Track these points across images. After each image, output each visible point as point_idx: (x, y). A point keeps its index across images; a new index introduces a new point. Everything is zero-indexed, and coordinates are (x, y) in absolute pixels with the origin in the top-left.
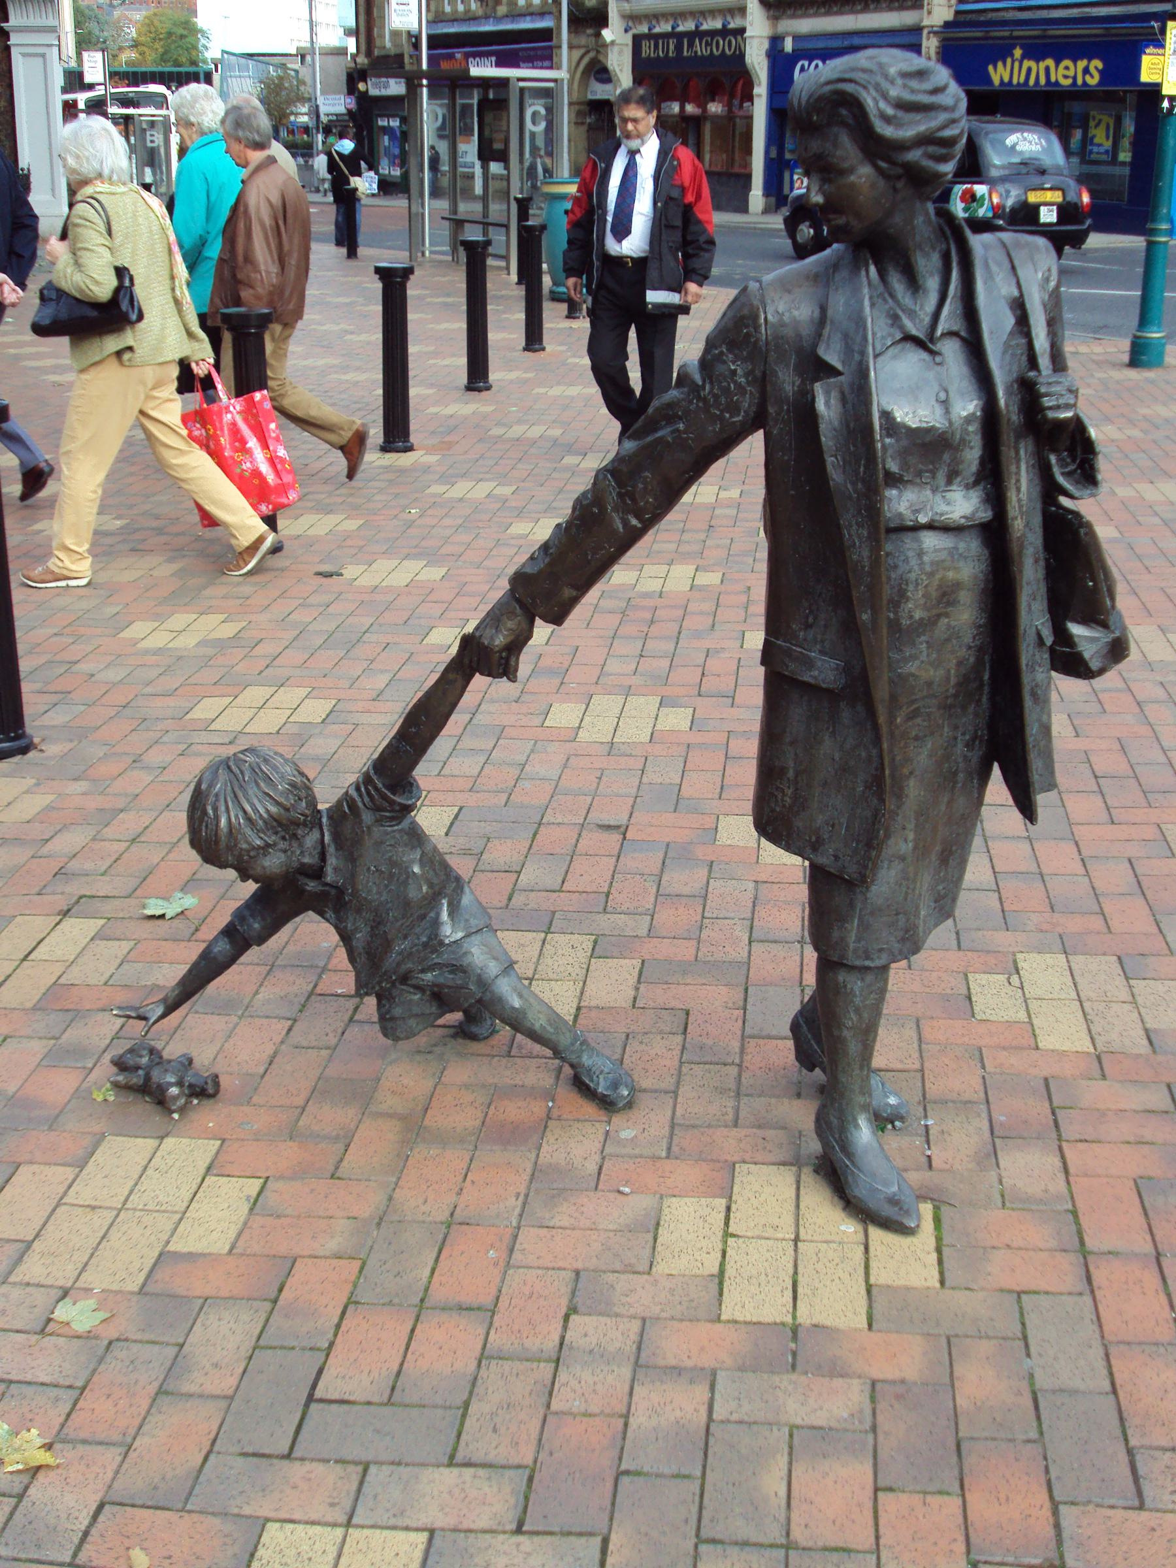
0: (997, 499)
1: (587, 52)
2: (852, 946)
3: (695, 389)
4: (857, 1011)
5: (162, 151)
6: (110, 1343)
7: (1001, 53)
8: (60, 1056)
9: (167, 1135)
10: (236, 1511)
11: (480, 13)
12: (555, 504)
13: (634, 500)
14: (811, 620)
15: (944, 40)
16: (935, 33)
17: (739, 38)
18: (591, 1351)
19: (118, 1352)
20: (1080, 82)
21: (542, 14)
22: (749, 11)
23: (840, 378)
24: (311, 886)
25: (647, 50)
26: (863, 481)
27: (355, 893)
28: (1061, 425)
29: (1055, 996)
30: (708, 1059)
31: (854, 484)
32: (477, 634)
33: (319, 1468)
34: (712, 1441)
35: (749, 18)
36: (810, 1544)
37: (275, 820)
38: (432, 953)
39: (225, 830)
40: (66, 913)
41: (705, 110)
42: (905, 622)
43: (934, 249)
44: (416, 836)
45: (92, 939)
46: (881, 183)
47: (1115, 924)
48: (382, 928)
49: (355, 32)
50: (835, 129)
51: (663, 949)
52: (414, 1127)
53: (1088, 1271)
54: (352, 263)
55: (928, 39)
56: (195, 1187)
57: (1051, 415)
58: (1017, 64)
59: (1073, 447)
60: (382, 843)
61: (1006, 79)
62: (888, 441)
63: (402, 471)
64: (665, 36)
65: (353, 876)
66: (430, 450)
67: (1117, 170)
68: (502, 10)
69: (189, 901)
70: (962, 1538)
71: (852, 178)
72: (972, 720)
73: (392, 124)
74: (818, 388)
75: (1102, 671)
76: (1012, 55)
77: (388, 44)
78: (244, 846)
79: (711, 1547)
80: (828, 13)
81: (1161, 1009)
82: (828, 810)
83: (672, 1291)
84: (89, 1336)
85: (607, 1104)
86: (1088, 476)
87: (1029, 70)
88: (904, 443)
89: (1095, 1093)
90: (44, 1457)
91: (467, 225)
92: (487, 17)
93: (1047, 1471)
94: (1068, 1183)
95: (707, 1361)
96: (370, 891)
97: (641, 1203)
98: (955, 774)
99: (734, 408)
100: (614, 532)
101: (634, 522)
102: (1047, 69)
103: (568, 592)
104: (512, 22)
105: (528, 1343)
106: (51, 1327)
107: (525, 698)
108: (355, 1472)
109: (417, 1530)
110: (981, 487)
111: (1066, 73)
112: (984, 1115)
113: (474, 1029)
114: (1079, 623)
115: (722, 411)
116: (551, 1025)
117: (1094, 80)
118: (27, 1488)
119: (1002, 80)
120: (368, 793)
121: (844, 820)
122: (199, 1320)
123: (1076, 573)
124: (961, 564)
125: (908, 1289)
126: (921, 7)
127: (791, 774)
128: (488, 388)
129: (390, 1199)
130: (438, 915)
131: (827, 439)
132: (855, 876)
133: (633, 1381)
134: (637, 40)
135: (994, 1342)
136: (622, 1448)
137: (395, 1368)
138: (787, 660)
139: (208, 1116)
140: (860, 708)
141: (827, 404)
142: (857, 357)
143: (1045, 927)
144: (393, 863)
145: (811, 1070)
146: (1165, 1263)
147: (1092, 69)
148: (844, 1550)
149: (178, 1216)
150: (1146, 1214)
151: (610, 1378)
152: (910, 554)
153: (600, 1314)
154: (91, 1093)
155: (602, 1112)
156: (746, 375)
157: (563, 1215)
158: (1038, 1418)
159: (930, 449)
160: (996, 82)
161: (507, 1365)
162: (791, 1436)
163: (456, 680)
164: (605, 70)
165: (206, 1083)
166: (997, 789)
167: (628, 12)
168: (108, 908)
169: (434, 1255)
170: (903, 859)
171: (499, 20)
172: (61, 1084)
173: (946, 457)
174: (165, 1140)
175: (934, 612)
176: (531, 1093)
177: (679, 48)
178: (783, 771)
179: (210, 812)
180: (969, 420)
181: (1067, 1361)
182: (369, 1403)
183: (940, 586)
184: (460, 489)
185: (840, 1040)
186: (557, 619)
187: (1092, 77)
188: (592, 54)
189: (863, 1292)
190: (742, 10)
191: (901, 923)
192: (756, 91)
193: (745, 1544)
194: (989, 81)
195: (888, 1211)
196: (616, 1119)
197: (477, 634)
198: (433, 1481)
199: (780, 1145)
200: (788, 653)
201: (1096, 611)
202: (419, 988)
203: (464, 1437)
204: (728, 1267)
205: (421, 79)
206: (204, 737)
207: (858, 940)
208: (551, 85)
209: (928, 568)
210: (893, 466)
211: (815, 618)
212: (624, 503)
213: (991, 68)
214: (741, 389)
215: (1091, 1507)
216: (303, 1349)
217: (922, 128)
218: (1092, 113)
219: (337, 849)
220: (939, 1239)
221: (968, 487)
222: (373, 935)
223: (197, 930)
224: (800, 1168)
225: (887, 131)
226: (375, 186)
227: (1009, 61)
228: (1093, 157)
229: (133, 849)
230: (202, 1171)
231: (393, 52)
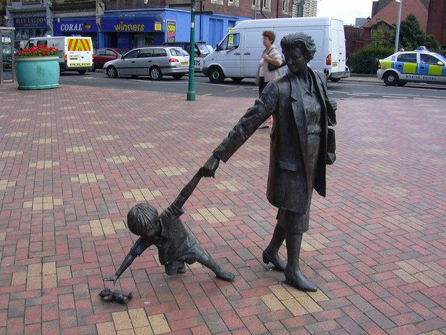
24: (157, 238)
85: (229, 280)
107: (14, 201)
117: (142, 30)
134: (15, 19)
159: (313, 115)
186: (225, 161)
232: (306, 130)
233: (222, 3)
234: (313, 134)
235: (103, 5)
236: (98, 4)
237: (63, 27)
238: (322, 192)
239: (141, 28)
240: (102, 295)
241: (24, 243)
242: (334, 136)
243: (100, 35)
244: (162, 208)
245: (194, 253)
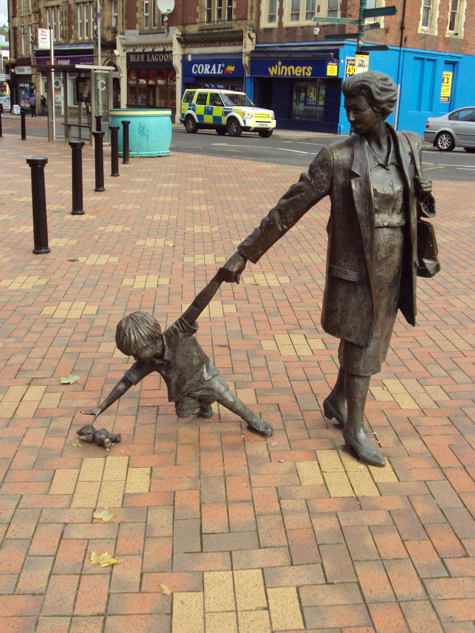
0: (407, 217)
1: (108, 59)
2: (361, 369)
3: (309, 182)
4: (361, 392)
6: (119, 524)
7: (273, 63)
8: (50, 432)
9: (107, 456)
10: (191, 570)
11: (63, 42)
12: (150, 233)
13: (286, 219)
14: (347, 258)
15: (251, 57)
16: (247, 55)
17: (170, 55)
18: (292, 510)
19: (122, 526)
20: (304, 75)
21: (89, 43)
22: (174, 44)
23: (360, 178)
24: (158, 361)
25: (132, 58)
26: (368, 211)
27: (175, 364)
29: (400, 392)
30: (291, 418)
31: (365, 213)
32: (226, 267)
33: (214, 555)
34: (344, 532)
35: (174, 47)
36: (389, 558)
37: (151, 336)
38: (201, 384)
39: (134, 341)
40: (29, 384)
41: (156, 83)
42: (379, 258)
43: (385, 136)
44: (195, 342)
45: (44, 393)
46: (374, 114)
47: (411, 369)
48: (183, 376)
50: (361, 97)
51: (260, 385)
52: (198, 447)
53: (444, 473)
54: (22, 142)
55: (245, 57)
56: (126, 472)
57: (425, 190)
58: (279, 68)
59: (428, 201)
60: (185, 344)
61: (276, 73)
62: (375, 198)
63: (84, 222)
64: (140, 53)
65: (174, 356)
66: (91, 214)
67: (318, 108)
68: (72, 41)
69: (76, 378)
70: (435, 552)
71: (365, 113)
72: (395, 291)
73: (26, 86)
74: (353, 182)
75: (434, 275)
76: (278, 64)
77: (24, 54)
78: (140, 346)
79: (357, 562)
81: (436, 394)
82: (353, 323)
83: (311, 490)
84: (110, 522)
85: (263, 434)
86: (432, 210)
87: (284, 70)
88: (380, 199)
89: (424, 421)
90: (114, 561)
91: (72, 127)
92: (66, 44)
93: (453, 530)
94: (427, 448)
95: (332, 509)
96: (179, 362)
97: (287, 465)
98: (391, 310)
99: (322, 188)
100: (279, 230)
101: (285, 227)
102: (291, 70)
103: (260, 252)
104: (76, 46)
105: (269, 510)
106: (94, 521)
108: (228, 555)
109: (257, 569)
110: (401, 214)
111: (299, 71)
112: (392, 430)
113: (206, 414)
114: (426, 259)
115: (318, 189)
116: (243, 408)
117: (309, 74)
118: (112, 571)
119: (274, 73)
120: (182, 326)
121: (359, 326)
122: (148, 514)
124: (396, 239)
125: (389, 483)
126: (242, 45)
127: (339, 311)
128: (104, 190)
129: (200, 470)
130: (203, 370)
131: (356, 198)
132: (364, 344)
133: (310, 518)
134: (128, 55)
135: (422, 496)
136: (316, 538)
137: (227, 522)
138: (338, 273)
139: (118, 448)
140: (365, 288)
141: (355, 186)
142: (365, 171)
143: (388, 371)
144: (188, 352)
145: (330, 418)
146: (467, 469)
147: (308, 70)
148: (400, 559)
149: (124, 482)
150: (456, 456)
151: (302, 517)
152: (381, 236)
153: (290, 499)
154: (72, 444)
155: (262, 438)
156: (326, 177)
157: (263, 470)
158: (445, 516)
159: (387, 200)
160: (272, 74)
161: (266, 517)
162: (369, 528)
163: (216, 284)
165: (117, 437)
167: (125, 44)
168: (46, 381)
169: (224, 486)
170: (377, 338)
171: (71, 45)
172: (57, 443)
173: (392, 204)
174: (107, 458)
175: (388, 255)
176: (235, 433)
177: (145, 58)
178: (336, 311)
179: (128, 335)
180: (399, 191)
181: (448, 499)
182: (223, 533)
183: (390, 247)
184: (110, 229)
185: (355, 403)
187: (308, 73)
188: (110, 60)
189: (374, 485)
190: (171, 44)
191: (376, 361)
192: (177, 75)
193: (368, 560)
194: (270, 74)
195: (374, 460)
196: (268, 439)
197: (226, 267)
198: (256, 553)
199: (328, 444)
200: (339, 270)
201: (432, 256)
202: (194, 398)
203: (260, 540)
204: (327, 481)
205: (51, 68)
206: (52, 321)
207: (363, 367)
208: (108, 72)
209: (386, 240)
210: (376, 207)
211: (349, 258)
212: (282, 220)
213: (269, 69)
214: (325, 182)
215: (471, 539)
216: (192, 519)
217: (388, 96)
218: (308, 87)
219: (168, 347)
220: (392, 467)
221: (398, 214)
222: (179, 378)
223: (84, 387)
224: (337, 450)
226: (19, 111)
227: (276, 66)
228: (309, 103)
229: (45, 360)
230: (126, 467)
231: (26, 57)
232: (371, 221)
233: (436, 33)
234: (387, 227)
235: (253, 35)
236: (246, 35)
237: (196, 69)
238: (411, 318)
239: (305, 71)
240: (80, 433)
241: (18, 359)
242: (44, 179)
243: (248, 81)
244: (167, 320)
245: (212, 389)
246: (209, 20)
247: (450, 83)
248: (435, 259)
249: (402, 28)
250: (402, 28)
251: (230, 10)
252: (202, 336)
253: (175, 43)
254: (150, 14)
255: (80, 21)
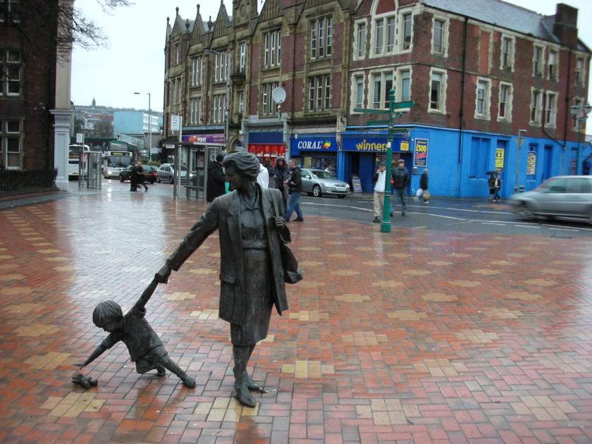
5: (455, 17)
7: (360, 140)
28: (280, 227)
49: (162, 128)
68: (209, 123)
74: (228, 219)
80: (308, 128)
86: (288, 238)
113: (162, 374)
123: (288, 262)
131: (230, 230)
159: (253, 232)
164: (240, 142)
166: (274, 308)
194: (357, 149)
225: (240, 167)
233: (489, 118)
236: (339, 119)
237: (301, 145)
246: (312, 108)
247: (503, 157)
248: (296, 272)
249: (461, 115)
250: (461, 115)
251: (327, 100)
252: (149, 317)
253: (285, 125)
254: (268, 104)
255: (215, 109)
